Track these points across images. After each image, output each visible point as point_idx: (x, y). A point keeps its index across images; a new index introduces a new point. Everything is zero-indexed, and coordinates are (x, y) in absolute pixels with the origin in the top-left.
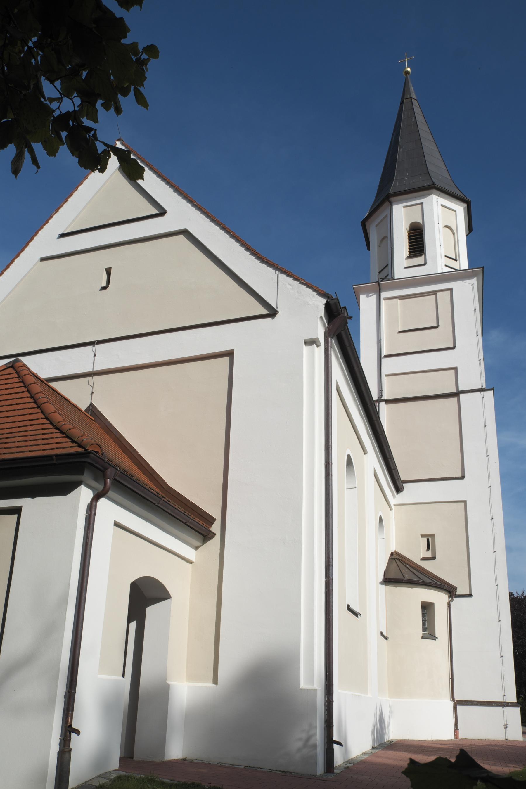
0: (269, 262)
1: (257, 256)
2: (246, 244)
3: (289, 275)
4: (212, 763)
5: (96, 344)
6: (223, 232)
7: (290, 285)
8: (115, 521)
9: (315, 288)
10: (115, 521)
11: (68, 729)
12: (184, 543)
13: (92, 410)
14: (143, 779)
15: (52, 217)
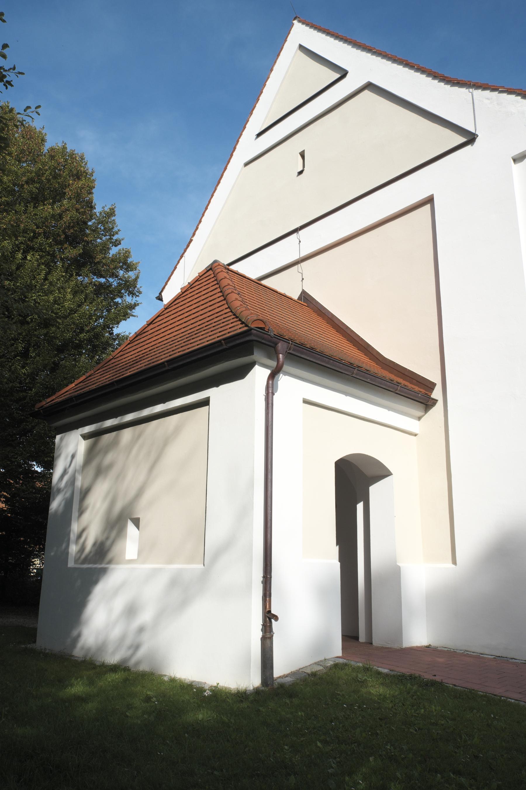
0: (461, 82)
1: (446, 80)
2: (433, 72)
3: (484, 87)
4: (458, 651)
5: (299, 231)
6: (406, 69)
7: (488, 99)
8: (303, 398)
9: (517, 92)
10: (303, 398)
11: (268, 615)
12: (399, 414)
13: (305, 297)
14: (359, 667)
15: (248, 121)
